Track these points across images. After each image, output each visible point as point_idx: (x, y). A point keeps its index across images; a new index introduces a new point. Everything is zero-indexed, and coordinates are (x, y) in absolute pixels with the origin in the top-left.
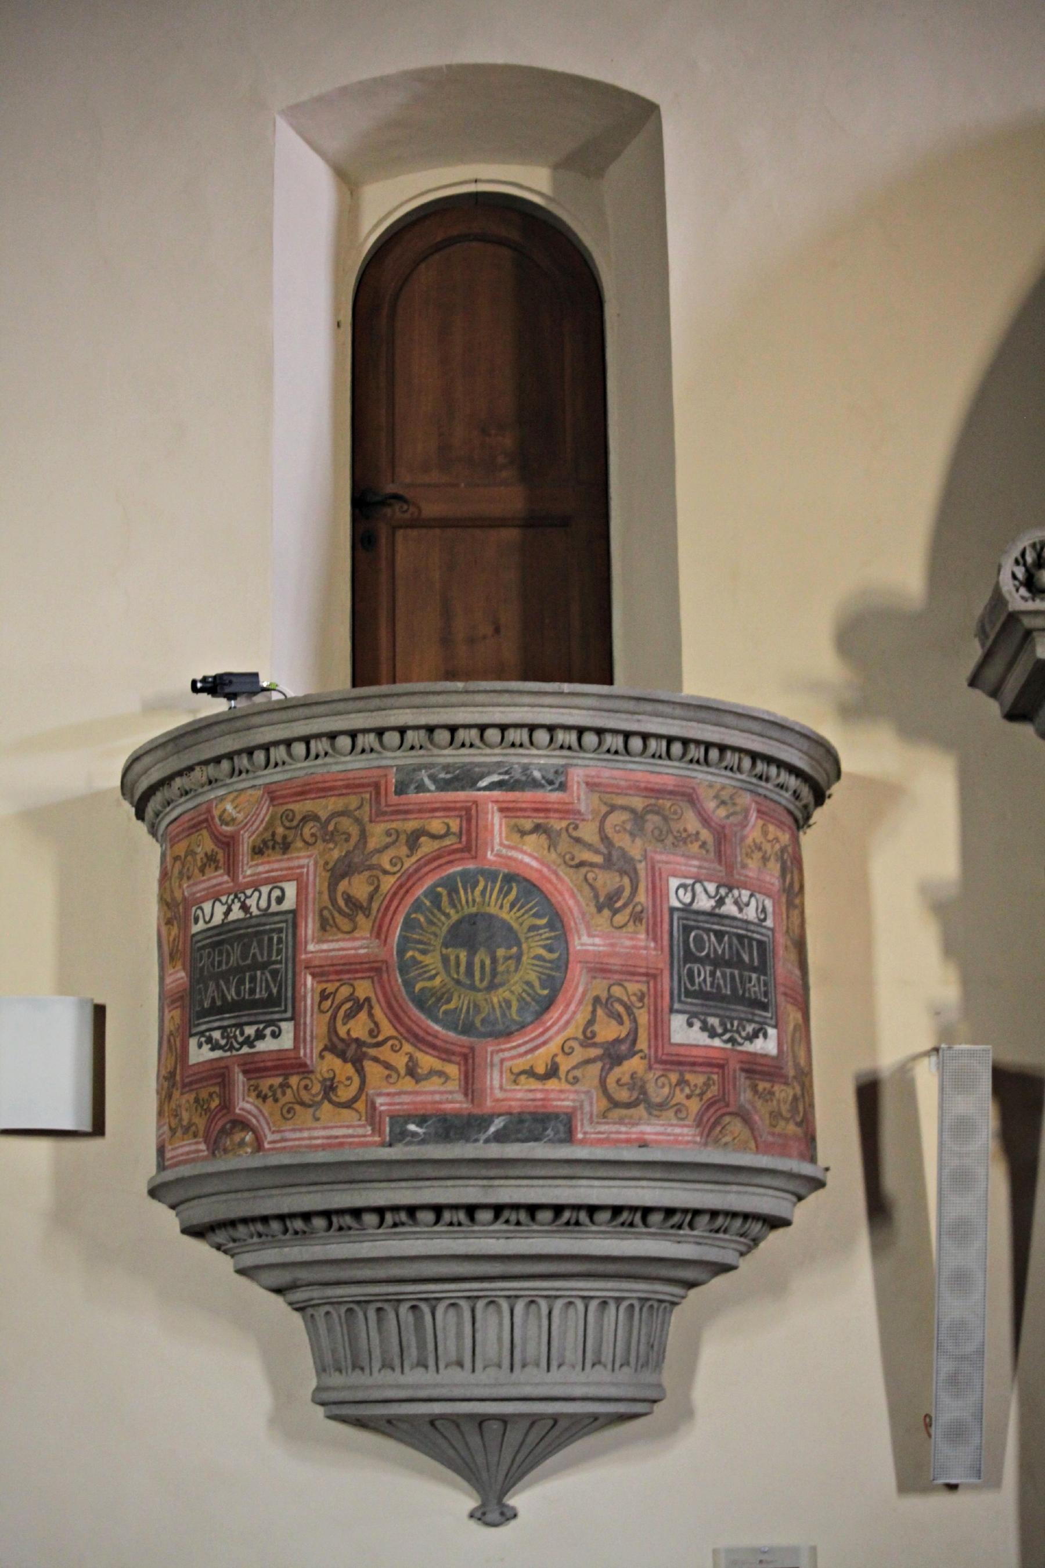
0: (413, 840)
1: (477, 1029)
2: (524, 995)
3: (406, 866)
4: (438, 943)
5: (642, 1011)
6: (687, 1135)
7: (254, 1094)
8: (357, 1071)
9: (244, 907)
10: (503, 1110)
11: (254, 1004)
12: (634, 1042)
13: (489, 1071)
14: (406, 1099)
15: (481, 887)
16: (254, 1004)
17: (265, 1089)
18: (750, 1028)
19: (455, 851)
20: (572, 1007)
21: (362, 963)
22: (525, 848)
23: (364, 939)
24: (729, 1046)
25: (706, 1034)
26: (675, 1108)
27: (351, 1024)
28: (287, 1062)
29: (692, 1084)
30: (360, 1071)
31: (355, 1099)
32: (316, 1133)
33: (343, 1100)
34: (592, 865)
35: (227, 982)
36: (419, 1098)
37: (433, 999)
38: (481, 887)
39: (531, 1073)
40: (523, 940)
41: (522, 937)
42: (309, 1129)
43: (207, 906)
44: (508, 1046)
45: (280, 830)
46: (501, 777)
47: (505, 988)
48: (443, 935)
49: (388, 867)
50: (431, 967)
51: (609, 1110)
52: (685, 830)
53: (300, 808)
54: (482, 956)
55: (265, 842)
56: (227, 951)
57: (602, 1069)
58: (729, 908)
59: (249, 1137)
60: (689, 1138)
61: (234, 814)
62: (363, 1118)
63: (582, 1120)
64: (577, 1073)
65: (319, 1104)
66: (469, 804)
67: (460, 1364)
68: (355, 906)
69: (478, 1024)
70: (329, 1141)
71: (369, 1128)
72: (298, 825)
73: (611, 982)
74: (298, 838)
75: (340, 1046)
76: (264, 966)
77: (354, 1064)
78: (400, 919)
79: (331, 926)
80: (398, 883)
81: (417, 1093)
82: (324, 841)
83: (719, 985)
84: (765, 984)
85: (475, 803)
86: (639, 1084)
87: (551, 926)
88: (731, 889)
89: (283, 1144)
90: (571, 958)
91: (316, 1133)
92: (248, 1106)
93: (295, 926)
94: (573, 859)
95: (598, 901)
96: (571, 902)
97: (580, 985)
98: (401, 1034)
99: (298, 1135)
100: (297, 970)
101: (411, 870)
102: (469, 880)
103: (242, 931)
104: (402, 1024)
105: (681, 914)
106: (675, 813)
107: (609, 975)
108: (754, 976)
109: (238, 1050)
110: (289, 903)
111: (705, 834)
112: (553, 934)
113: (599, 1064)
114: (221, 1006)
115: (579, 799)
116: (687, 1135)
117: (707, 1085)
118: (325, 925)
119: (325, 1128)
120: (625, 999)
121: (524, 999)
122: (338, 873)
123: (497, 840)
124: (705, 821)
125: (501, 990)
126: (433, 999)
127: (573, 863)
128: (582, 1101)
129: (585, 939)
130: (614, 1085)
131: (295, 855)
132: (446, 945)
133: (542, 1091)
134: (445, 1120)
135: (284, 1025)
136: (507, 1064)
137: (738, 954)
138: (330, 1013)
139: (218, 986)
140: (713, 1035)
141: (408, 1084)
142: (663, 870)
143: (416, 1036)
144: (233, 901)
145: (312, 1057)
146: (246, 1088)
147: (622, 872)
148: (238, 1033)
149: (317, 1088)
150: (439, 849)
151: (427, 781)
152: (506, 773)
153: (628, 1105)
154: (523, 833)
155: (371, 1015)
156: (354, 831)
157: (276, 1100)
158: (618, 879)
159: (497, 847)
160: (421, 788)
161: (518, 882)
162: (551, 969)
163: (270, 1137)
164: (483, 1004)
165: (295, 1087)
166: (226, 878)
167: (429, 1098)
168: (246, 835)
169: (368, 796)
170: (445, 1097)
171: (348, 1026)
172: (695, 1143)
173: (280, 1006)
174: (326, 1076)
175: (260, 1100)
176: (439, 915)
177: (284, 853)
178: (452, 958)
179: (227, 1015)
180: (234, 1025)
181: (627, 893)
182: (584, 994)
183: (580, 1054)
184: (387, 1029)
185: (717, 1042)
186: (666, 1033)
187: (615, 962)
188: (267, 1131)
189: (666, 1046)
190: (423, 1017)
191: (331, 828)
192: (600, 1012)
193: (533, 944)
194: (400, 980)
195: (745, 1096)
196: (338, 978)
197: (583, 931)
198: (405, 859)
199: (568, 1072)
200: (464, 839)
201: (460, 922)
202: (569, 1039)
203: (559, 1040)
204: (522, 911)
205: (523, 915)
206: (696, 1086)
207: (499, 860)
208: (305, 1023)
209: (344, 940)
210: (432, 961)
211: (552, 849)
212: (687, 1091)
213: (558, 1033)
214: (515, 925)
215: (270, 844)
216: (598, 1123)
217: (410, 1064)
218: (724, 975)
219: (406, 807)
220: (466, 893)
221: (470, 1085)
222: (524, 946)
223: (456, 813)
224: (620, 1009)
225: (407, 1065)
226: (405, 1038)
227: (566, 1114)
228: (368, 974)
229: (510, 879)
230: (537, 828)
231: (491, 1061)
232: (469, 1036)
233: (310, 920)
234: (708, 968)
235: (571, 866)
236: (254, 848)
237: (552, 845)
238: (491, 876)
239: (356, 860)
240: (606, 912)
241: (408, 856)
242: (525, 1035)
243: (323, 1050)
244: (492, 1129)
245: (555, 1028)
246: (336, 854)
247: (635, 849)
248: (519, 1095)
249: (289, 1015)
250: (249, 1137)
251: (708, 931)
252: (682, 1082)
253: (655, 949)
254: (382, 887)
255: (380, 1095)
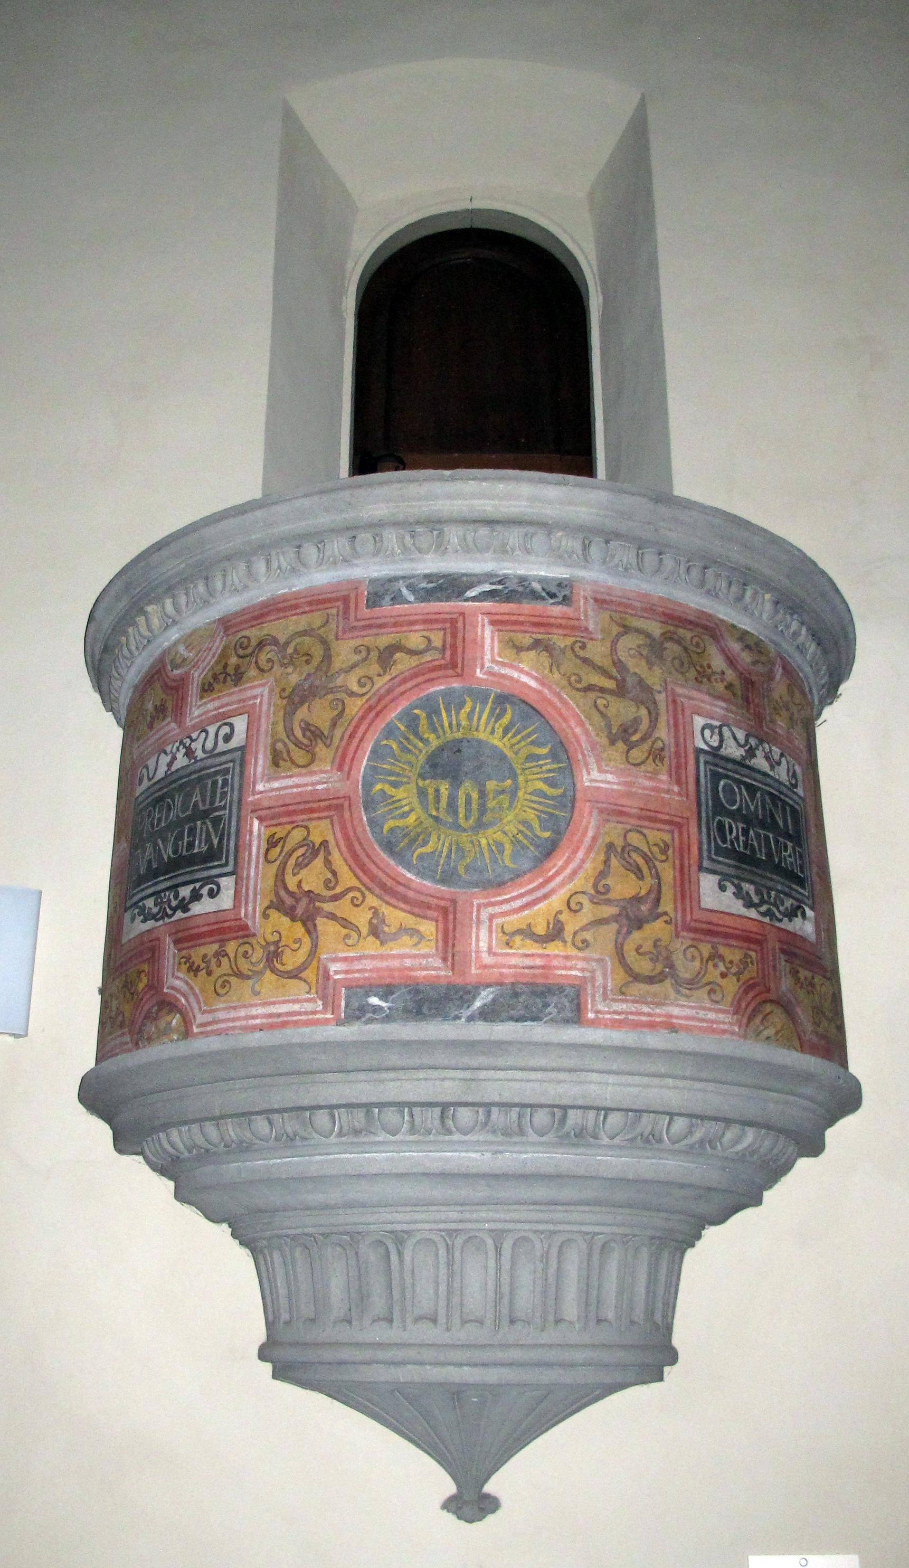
0: (386, 656)
1: (459, 876)
2: (520, 837)
3: (376, 686)
4: (413, 775)
5: (665, 865)
6: (724, 1023)
7: (184, 967)
8: (308, 932)
9: (189, 753)
10: (493, 979)
11: (191, 860)
12: (658, 900)
13: (474, 930)
14: (368, 964)
15: (467, 708)
16: (191, 860)
17: (198, 961)
18: (789, 903)
19: (440, 667)
20: (580, 855)
21: (320, 801)
22: (521, 666)
23: (323, 772)
24: (767, 920)
25: (740, 902)
26: (708, 988)
27: (303, 873)
28: (226, 925)
29: (727, 960)
30: (311, 930)
31: (303, 967)
32: (254, 1011)
33: (289, 968)
34: (602, 690)
35: (165, 841)
36: (385, 964)
37: (406, 840)
38: (467, 708)
39: (527, 933)
40: (519, 772)
41: (518, 768)
42: (244, 1006)
43: (151, 763)
44: (499, 898)
45: (233, 660)
46: (494, 587)
47: (496, 828)
48: (419, 765)
49: (355, 688)
50: (404, 803)
51: (626, 984)
52: (709, 666)
53: (254, 634)
54: (468, 787)
55: (215, 677)
56: (169, 805)
57: (618, 932)
58: (759, 762)
59: (176, 1020)
60: (726, 1027)
61: (186, 654)
62: (313, 991)
63: (594, 996)
64: (588, 936)
65: (260, 973)
66: (455, 616)
67: (434, 1320)
68: (314, 734)
69: (461, 871)
70: (270, 1020)
71: (320, 1003)
72: (253, 652)
73: (628, 827)
74: (253, 665)
75: (289, 901)
76: (205, 815)
77: (304, 924)
78: (369, 747)
79: (284, 760)
80: (366, 706)
81: (382, 957)
82: (283, 665)
83: (752, 845)
84: (801, 857)
85: (462, 614)
86: (664, 954)
87: (554, 756)
88: (761, 741)
89: (215, 1027)
90: (579, 795)
91: (254, 1011)
92: (178, 983)
93: (243, 763)
94: (579, 681)
95: (610, 732)
96: (578, 730)
97: (589, 823)
98: (364, 885)
99: (233, 1014)
100: (243, 814)
101: (382, 691)
102: (454, 701)
103: (184, 780)
104: (365, 871)
105: (709, 758)
106: (698, 645)
107: (624, 819)
108: (790, 844)
109: (170, 916)
110: (238, 739)
111: (730, 675)
112: (555, 766)
113: (614, 926)
114: (157, 868)
115: (586, 616)
116: (724, 1023)
117: (744, 963)
118: (276, 759)
119: (265, 1004)
120: (646, 850)
121: (519, 842)
122: (295, 699)
123: (488, 656)
124: (731, 661)
125: (490, 831)
126: (406, 840)
127: (579, 686)
128: (593, 972)
129: (595, 774)
130: (633, 953)
131: (247, 685)
132: (422, 776)
133: (540, 956)
134: (417, 992)
135: (224, 881)
136: (498, 921)
137: (772, 815)
138: (278, 863)
139: (155, 845)
140: (749, 904)
141: (371, 946)
142: (686, 705)
143: (383, 886)
144: (178, 749)
145: (254, 917)
146: (177, 959)
147: (639, 702)
148: (172, 897)
149: (258, 954)
150: (417, 666)
151: (405, 591)
152: (500, 582)
153: (650, 980)
154: (519, 649)
155: (328, 862)
156: (318, 652)
157: (209, 973)
158: (634, 709)
159: (487, 664)
160: (397, 598)
161: (512, 704)
162: (555, 807)
163: (200, 1018)
164: (468, 847)
165: (232, 955)
166: (173, 725)
167: (396, 963)
168: (196, 674)
169: (334, 611)
170: (416, 962)
171: (299, 877)
172: (733, 1033)
173: (221, 859)
174: (270, 938)
175: (192, 973)
176: (416, 741)
177: (236, 685)
178: (431, 791)
179: (162, 878)
180: (168, 889)
181: (644, 726)
182: (594, 839)
183: (588, 912)
184: (347, 878)
185: (753, 913)
186: (695, 895)
187: (632, 806)
188: (196, 1011)
189: (696, 910)
190: (392, 862)
191: (290, 650)
192: (614, 862)
193: (530, 777)
194: (365, 819)
195: (786, 984)
196: (289, 819)
197: (591, 760)
198: (376, 678)
199: (575, 933)
200: (448, 653)
201: (441, 749)
202: (576, 893)
203: (563, 893)
204: (519, 737)
205: (519, 742)
206: (731, 962)
207: (491, 678)
208: (248, 876)
209: (300, 775)
210: (405, 795)
211: (554, 669)
212: (722, 968)
213: (562, 884)
214: (509, 753)
215: (221, 677)
216: (614, 1000)
217: (375, 921)
218: (758, 835)
219: (378, 621)
220: (449, 716)
221: (449, 943)
222: (521, 779)
223: (439, 626)
224: (640, 861)
225: (370, 922)
226: (369, 889)
227: (573, 986)
228: (325, 814)
229: (503, 700)
230: (536, 644)
231: (478, 918)
232: (449, 886)
233: (261, 756)
234: (740, 825)
235: (578, 690)
236: (203, 685)
237: (555, 664)
238: (481, 697)
239: (317, 683)
240: (620, 745)
241: (379, 675)
242: (521, 885)
243: (268, 908)
244: (478, 1004)
245: (559, 879)
246: (294, 679)
247: (654, 678)
248: (513, 961)
249: (229, 869)
250: (176, 1020)
251: (739, 782)
252: (715, 956)
253: (679, 794)
254: (347, 710)
255: (334, 960)
